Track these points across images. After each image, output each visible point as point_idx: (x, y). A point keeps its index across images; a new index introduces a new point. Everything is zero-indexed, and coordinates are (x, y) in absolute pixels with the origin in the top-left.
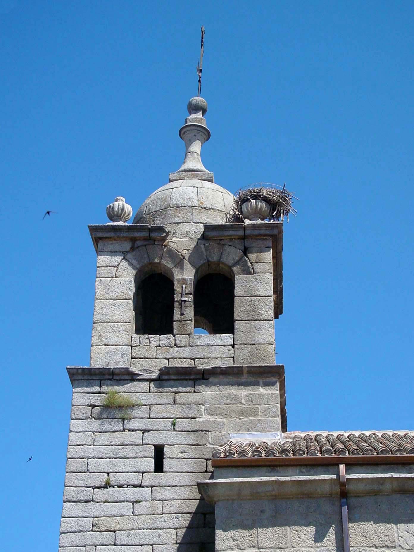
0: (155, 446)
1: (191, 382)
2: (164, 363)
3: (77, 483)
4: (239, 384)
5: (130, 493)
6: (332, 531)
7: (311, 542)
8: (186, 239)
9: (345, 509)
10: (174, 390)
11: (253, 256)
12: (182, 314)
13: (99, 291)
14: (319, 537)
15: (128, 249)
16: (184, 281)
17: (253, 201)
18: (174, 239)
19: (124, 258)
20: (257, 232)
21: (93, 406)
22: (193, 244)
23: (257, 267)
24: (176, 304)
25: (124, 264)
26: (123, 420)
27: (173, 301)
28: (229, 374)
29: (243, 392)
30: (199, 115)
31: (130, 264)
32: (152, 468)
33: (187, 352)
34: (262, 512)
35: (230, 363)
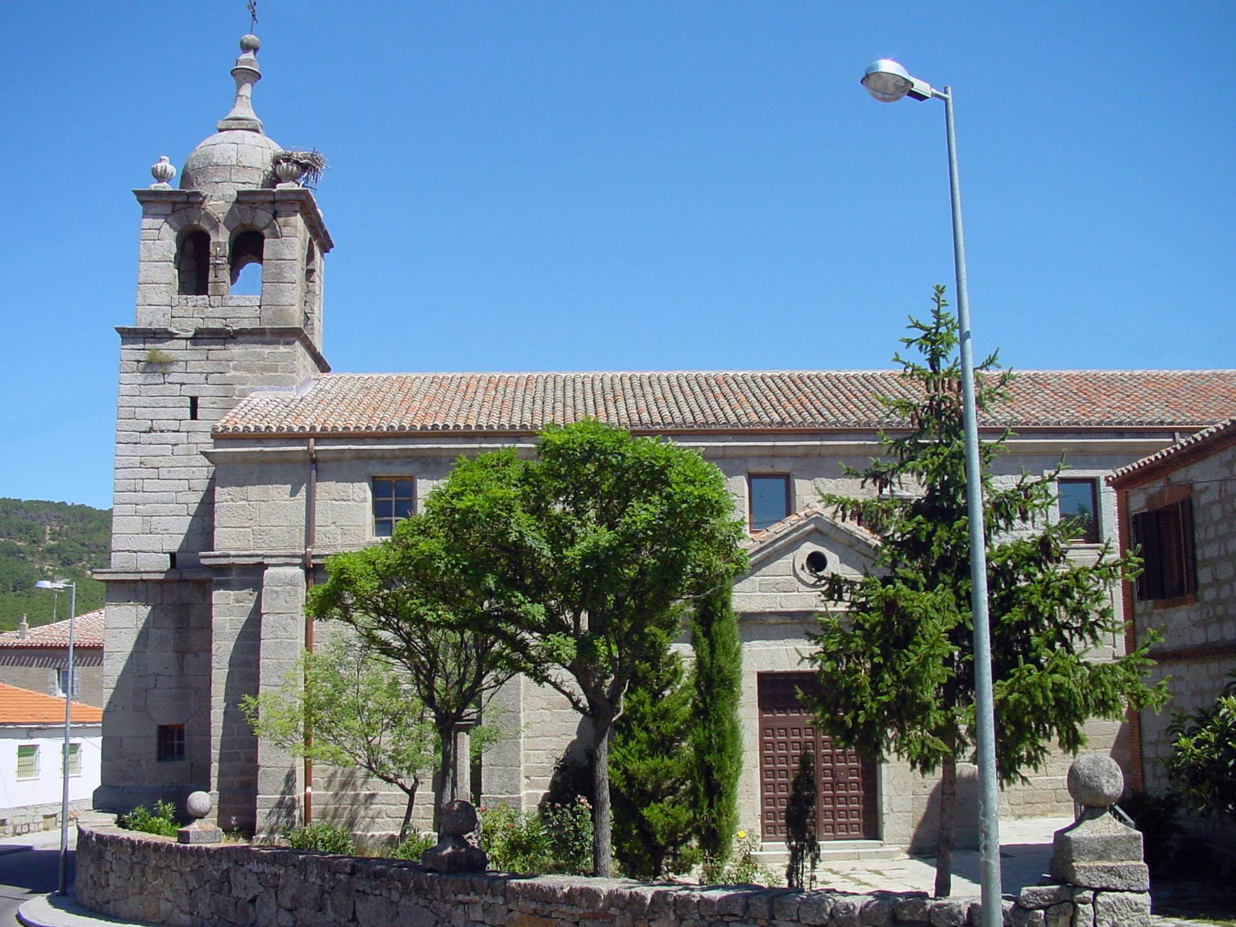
0: (191, 397)
1: (222, 341)
2: (201, 324)
3: (126, 428)
4: (263, 343)
5: (170, 437)
6: (304, 488)
7: (287, 497)
8: (222, 202)
9: (314, 473)
10: (207, 347)
11: (281, 220)
12: (216, 276)
13: (143, 254)
14: (293, 493)
15: (169, 212)
16: (219, 244)
17: (284, 165)
18: (211, 203)
19: (166, 221)
20: (285, 197)
21: (139, 362)
22: (228, 208)
23: (285, 231)
24: (211, 266)
25: (166, 226)
26: (164, 374)
27: (208, 264)
28: (255, 334)
29: (266, 350)
30: (250, 55)
31: (171, 226)
32: (189, 416)
33: (219, 312)
34: (251, 473)
35: (255, 325)
